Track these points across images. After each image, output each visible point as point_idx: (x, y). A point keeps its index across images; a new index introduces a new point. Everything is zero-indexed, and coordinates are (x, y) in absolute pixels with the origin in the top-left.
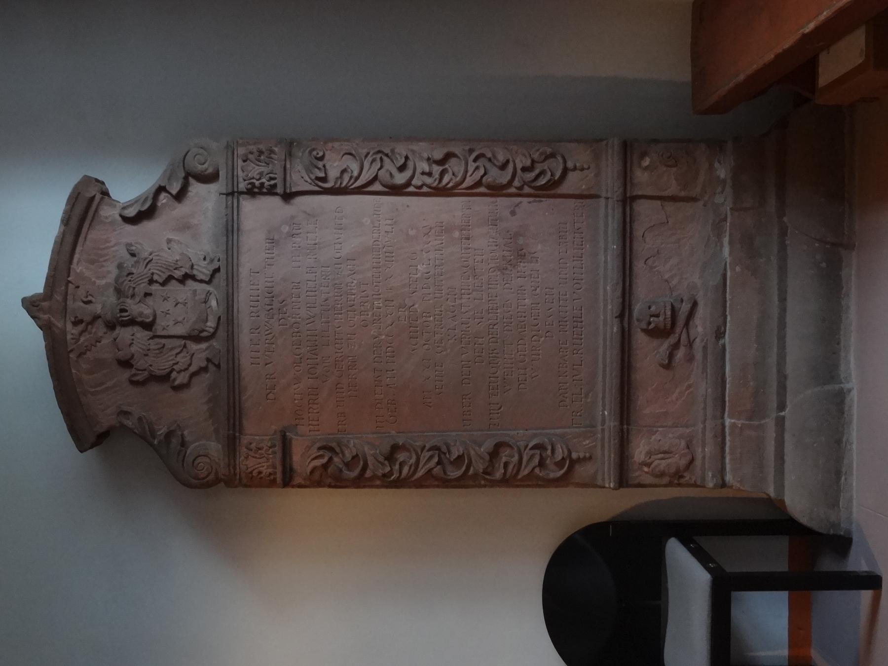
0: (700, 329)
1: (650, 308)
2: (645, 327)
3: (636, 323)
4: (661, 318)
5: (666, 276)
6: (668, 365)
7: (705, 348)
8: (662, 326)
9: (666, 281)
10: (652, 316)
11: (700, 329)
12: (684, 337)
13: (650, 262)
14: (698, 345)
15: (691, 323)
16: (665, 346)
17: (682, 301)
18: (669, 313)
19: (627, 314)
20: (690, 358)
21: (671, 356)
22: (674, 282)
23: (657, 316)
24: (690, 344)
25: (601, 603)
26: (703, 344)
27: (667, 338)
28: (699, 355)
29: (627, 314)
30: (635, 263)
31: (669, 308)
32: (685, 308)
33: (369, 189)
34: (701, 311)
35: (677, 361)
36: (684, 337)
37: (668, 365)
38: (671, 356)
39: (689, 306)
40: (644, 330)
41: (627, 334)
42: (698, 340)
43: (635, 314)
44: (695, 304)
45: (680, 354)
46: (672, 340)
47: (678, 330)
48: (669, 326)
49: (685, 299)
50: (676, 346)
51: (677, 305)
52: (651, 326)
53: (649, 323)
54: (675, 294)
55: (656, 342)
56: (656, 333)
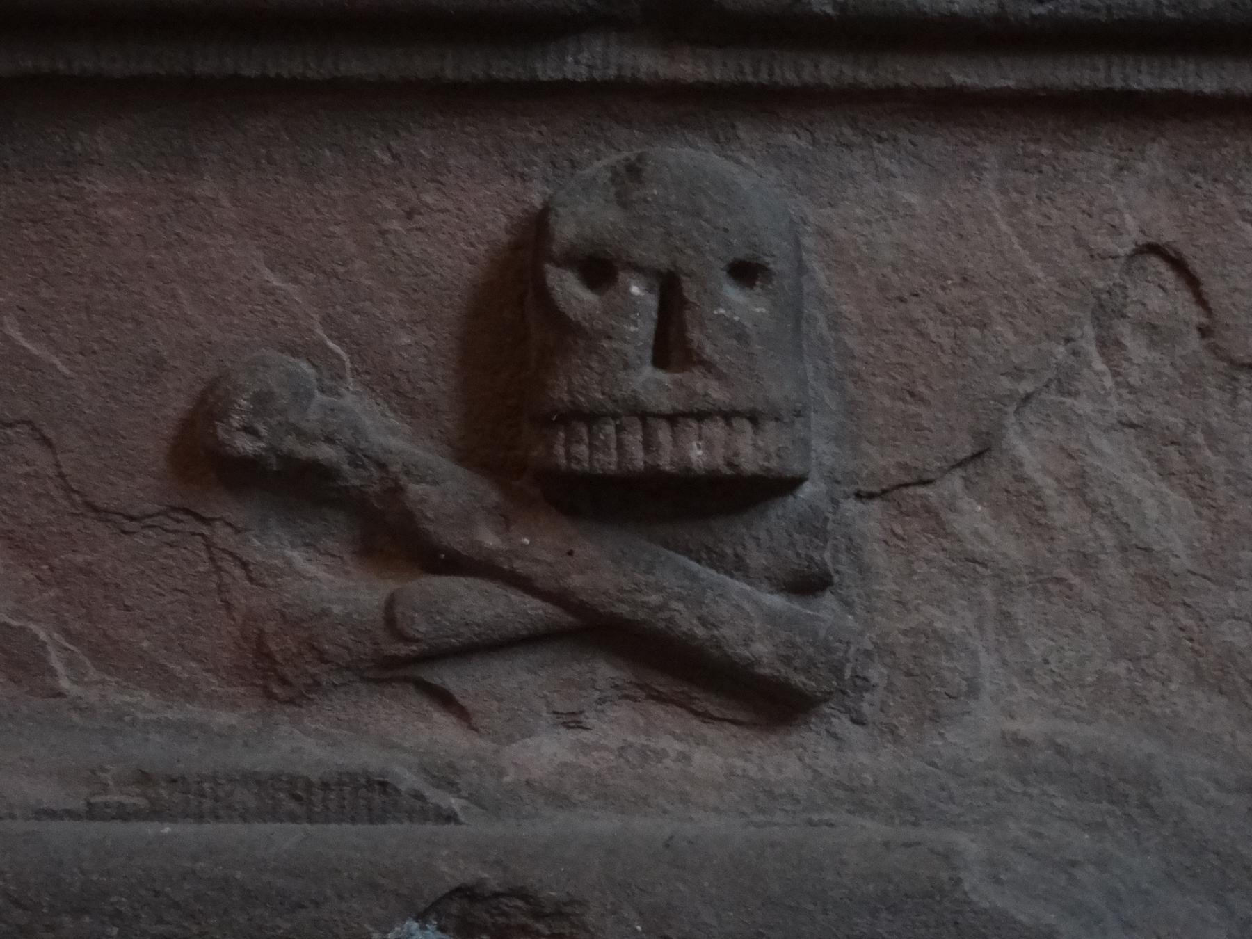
0: (546, 751)
1: (746, 272)
2: (566, 231)
3: (602, 163)
4: (650, 383)
5: (1026, 448)
6: (216, 466)
7: (371, 796)
8: (578, 382)
9: (984, 451)
10: (669, 289)
11: (546, 751)
12: (472, 603)
13: (1159, 295)
14: (400, 736)
15: (605, 671)
16: (390, 433)
17: (809, 584)
18: (699, 452)
19: (690, 67)
20: (279, 667)
21: (298, 486)
22: (974, 518)
23: (670, 347)
24: (407, 665)
25: (466, 927)
26: (408, 779)
27: (465, 457)
28: (308, 743)
29: (690, 67)
30: (1155, 157)
31: (751, 451)
32: (741, 612)
33: (534, 608)
34: (704, 771)
35: (256, 548)
36: (472, 603)
37: (216, 466)
38: (298, 486)
39: (762, 651)
40: (534, 232)
41: (505, 67)
42: (442, 734)
43: (687, 156)
44: (771, 701)
45: (323, 579)
46: (445, 492)
47: (541, 545)
48: (583, 453)
49: (826, 608)
50: (391, 534)
51: (767, 534)
52: (570, 290)
53: (599, 270)
54: (869, 520)
55: (420, 344)
56: (512, 339)
